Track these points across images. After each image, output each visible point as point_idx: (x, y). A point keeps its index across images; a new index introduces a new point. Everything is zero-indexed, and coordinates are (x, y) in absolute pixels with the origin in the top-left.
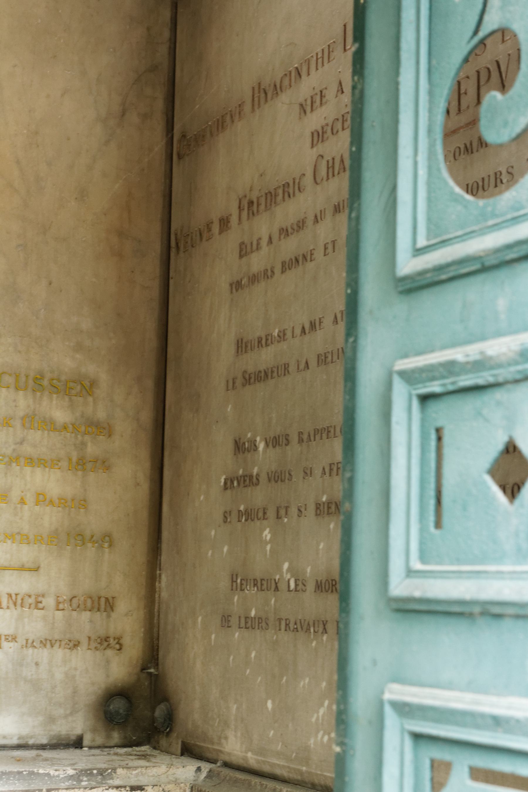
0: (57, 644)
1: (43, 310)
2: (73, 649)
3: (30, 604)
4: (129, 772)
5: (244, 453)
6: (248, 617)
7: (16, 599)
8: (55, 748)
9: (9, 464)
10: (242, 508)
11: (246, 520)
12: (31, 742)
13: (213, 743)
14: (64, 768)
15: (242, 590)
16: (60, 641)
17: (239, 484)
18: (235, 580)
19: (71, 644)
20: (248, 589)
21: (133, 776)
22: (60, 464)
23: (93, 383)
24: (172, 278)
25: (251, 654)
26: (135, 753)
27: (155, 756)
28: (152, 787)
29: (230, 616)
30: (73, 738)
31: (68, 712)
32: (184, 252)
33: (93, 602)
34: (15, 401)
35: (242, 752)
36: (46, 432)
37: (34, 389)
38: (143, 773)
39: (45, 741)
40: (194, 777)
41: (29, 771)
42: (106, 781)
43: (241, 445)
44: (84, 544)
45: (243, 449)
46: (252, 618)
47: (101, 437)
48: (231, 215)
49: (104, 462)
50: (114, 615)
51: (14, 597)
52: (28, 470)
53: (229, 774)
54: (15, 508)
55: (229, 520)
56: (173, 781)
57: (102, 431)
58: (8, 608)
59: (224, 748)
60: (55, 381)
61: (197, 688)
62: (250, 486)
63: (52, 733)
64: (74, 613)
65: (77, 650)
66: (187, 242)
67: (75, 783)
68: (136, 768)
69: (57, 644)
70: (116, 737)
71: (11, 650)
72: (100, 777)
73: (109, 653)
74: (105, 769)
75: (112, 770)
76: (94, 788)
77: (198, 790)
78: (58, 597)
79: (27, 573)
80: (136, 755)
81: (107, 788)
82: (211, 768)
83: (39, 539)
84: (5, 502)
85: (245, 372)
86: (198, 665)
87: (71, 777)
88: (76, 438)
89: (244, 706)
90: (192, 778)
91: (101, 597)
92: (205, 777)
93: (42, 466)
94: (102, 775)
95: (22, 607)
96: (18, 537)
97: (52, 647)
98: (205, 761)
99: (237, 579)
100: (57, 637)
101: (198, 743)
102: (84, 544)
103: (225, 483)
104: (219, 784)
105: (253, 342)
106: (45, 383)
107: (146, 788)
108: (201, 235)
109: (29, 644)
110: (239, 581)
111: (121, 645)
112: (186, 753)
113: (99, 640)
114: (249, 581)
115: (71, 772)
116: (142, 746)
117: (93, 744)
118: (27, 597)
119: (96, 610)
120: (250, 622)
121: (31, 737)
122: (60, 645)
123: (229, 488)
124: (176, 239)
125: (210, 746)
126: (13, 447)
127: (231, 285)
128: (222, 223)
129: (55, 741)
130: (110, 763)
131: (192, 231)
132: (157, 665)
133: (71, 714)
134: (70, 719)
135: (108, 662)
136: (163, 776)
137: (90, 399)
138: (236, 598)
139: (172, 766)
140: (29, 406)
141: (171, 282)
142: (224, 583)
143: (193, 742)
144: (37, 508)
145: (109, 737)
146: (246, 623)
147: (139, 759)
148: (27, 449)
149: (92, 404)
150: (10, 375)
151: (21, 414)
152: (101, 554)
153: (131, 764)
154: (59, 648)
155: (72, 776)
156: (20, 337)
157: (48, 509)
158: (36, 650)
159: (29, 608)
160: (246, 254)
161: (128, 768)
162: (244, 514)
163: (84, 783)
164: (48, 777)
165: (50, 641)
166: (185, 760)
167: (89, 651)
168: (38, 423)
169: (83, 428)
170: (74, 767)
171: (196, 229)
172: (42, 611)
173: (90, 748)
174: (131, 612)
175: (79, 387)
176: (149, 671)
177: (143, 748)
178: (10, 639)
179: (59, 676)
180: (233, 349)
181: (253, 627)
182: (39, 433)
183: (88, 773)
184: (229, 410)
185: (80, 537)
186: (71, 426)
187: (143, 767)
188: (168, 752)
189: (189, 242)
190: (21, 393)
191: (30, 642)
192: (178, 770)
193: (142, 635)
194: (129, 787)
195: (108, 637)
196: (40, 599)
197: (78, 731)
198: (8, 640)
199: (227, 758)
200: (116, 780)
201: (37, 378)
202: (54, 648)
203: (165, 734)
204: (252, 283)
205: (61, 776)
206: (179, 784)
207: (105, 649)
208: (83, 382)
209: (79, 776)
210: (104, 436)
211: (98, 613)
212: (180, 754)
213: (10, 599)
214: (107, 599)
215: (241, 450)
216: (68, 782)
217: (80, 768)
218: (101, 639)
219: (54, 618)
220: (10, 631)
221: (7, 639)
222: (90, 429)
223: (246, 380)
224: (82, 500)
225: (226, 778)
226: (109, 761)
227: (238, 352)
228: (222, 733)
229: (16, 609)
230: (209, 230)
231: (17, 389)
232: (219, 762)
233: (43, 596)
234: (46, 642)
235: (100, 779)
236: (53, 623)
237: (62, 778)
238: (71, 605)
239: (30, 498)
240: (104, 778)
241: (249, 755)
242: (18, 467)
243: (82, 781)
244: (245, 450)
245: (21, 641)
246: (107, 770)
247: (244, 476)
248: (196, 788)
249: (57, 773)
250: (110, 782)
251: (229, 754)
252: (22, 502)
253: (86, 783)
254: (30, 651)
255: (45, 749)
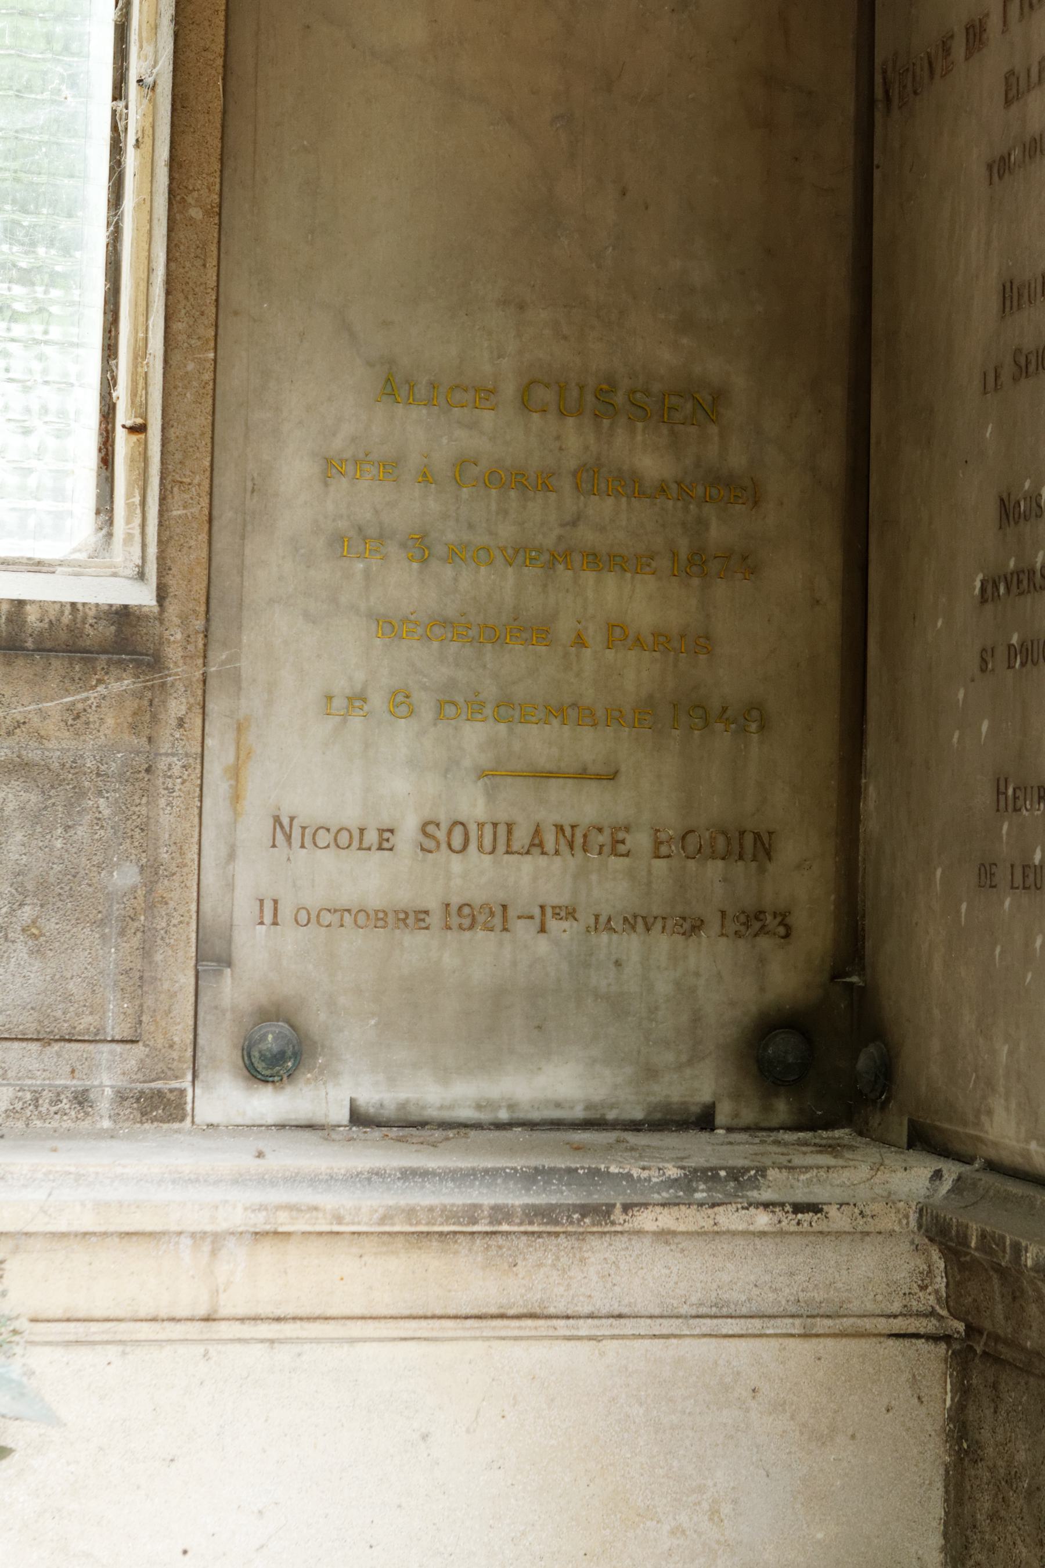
0: (659, 925)
1: (611, 249)
2: (691, 935)
3: (601, 847)
4: (793, 1175)
5: (1016, 523)
6: (1029, 866)
7: (573, 835)
8: (660, 1128)
9: (550, 565)
10: (1015, 640)
11: (1023, 664)
12: (611, 1115)
13: (965, 1124)
14: (661, 1165)
15: (1016, 810)
16: (664, 918)
17: (1008, 589)
18: (1002, 788)
19: (687, 926)
20: (1028, 807)
21: (800, 1184)
22: (654, 564)
23: (719, 396)
24: (878, 167)
25: (1034, 942)
26: (817, 1141)
27: (851, 1148)
28: (838, 1206)
29: (995, 864)
30: (695, 1109)
31: (684, 1058)
32: (900, 108)
33: (728, 840)
34: (558, 438)
35: (1018, 1141)
36: (624, 500)
37: (597, 413)
38: (822, 1179)
39: (638, 1115)
40: (928, 1189)
41: (589, 1168)
42: (745, 1192)
43: (1012, 505)
44: (707, 724)
45: (1016, 516)
46: (1035, 866)
47: (738, 507)
48: (987, 15)
49: (745, 558)
50: (771, 867)
51: (568, 832)
52: (589, 577)
53: (993, 1184)
54: (566, 655)
55: (990, 666)
56: (882, 1197)
57: (740, 495)
58: (557, 852)
59: (987, 1132)
60: (638, 395)
61: (936, 1012)
62: (1029, 592)
63: (652, 1099)
64: (691, 864)
65: (700, 936)
66: (905, 87)
67: (681, 1193)
68: (807, 1168)
69: (659, 925)
70: (782, 1109)
71: (565, 936)
72: (732, 1184)
73: (765, 942)
74: (743, 1168)
75: (757, 1171)
76: (719, 1205)
77: (932, 1215)
78: (658, 831)
79: (594, 784)
80: (815, 1145)
81: (746, 1205)
82: (960, 1174)
83: (615, 717)
84: (545, 643)
85: (1018, 351)
86: (937, 966)
87: (673, 1183)
88: (686, 509)
89: (1022, 1048)
90: (923, 1192)
91: (745, 831)
92: (949, 1191)
93: (617, 568)
94: (736, 1179)
95: (585, 851)
96: (573, 713)
97: (648, 930)
98: (953, 1159)
99: (1006, 788)
100: (656, 910)
101: (938, 1123)
102: (707, 724)
103: (983, 589)
104: (973, 1204)
105: (1033, 286)
106: (620, 398)
107: (825, 1207)
108: (930, 64)
109: (601, 924)
110: (1010, 791)
111: (788, 928)
112: (918, 1144)
113: (743, 918)
114: (1029, 790)
115: (673, 1172)
116: (837, 1129)
117: (735, 1123)
118: (594, 832)
119: (736, 858)
120: (1032, 876)
121: (612, 1107)
122: (664, 928)
123: (990, 599)
124: (885, 83)
125: (960, 1129)
126: (557, 531)
127: (990, 167)
128: (971, 36)
129: (658, 1116)
130: (759, 1157)
131: (914, 61)
132: (862, 971)
133: (690, 1062)
134: (688, 1072)
135: (762, 961)
136: (862, 1185)
137: (713, 430)
138: (1005, 827)
139: (882, 1167)
140: (587, 448)
141: (877, 174)
142: (984, 798)
143: (928, 1121)
144: (610, 654)
145: (767, 1108)
146: (1025, 876)
147: (821, 1152)
148: (587, 536)
149: (716, 439)
150: (547, 386)
151: (572, 464)
152: (743, 746)
153: (798, 1160)
154: (663, 932)
155: (676, 1180)
156: (565, 306)
157: (632, 655)
158: (615, 936)
159: (600, 853)
160: (1018, 96)
161: (791, 1169)
162: (1018, 652)
163: (699, 1196)
164: (627, 1182)
165: (644, 918)
166: (913, 1157)
167: (724, 939)
168: (608, 481)
169: (700, 490)
170: (680, 1164)
171: (922, 55)
172: (627, 860)
173: (730, 1130)
174: (808, 863)
175: (689, 406)
176: (848, 980)
177: (837, 1133)
178: (563, 914)
179: (663, 987)
180: (994, 304)
181: (1039, 886)
182: (610, 501)
183: (708, 1175)
184: (988, 435)
185: (700, 712)
186: (674, 486)
187: (822, 1167)
188: (883, 1141)
189: (909, 85)
190: (571, 421)
191: (603, 919)
192: (893, 1175)
193: (832, 907)
194: (790, 1204)
195: (761, 912)
196: (621, 835)
197: (706, 1096)
198: (558, 917)
199: (992, 1154)
200: (766, 1192)
201: (601, 390)
202: (652, 932)
203: (879, 1105)
204: (1030, 157)
205: (654, 1180)
206: (894, 1203)
207: (755, 936)
208: (697, 396)
209: (690, 1181)
210: (744, 504)
211: (740, 863)
212: (906, 1146)
213: (560, 836)
214: (757, 836)
215: (1011, 518)
216: (668, 1192)
217: (693, 1165)
218: (748, 916)
219: (649, 872)
220: (563, 899)
221: (559, 914)
222: (714, 491)
223: (1020, 367)
224: (700, 637)
225: (987, 1191)
226: (756, 1154)
227: (1004, 312)
228: (981, 1103)
229: (573, 855)
230: (947, 51)
231: (562, 414)
232: (978, 1161)
233: (627, 829)
234: (635, 922)
235: (733, 1188)
236: (649, 884)
237: (656, 1183)
238: (683, 848)
239: (594, 634)
240: (741, 1186)
241: (1033, 1146)
242: (570, 573)
243: (696, 1190)
244: (1019, 518)
245: (586, 918)
246: (747, 1170)
247: (1018, 573)
248: (929, 1211)
249: (645, 1174)
250: (754, 1195)
251: (995, 1144)
252: (580, 641)
253: (705, 1194)
254: (605, 937)
255: (639, 1130)
